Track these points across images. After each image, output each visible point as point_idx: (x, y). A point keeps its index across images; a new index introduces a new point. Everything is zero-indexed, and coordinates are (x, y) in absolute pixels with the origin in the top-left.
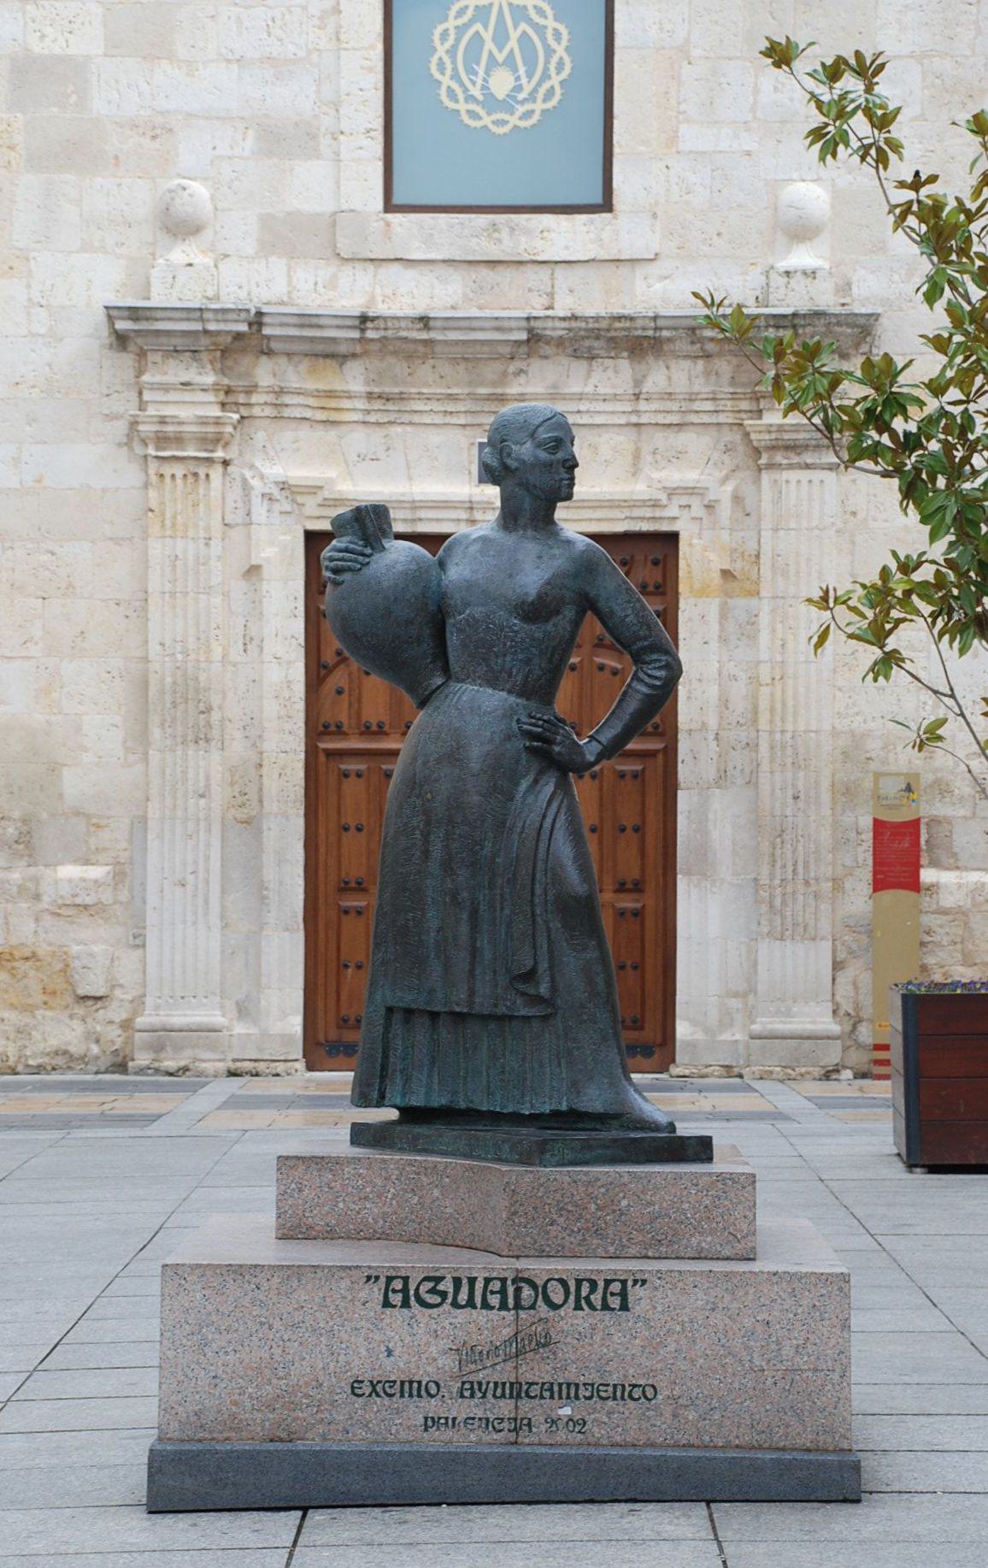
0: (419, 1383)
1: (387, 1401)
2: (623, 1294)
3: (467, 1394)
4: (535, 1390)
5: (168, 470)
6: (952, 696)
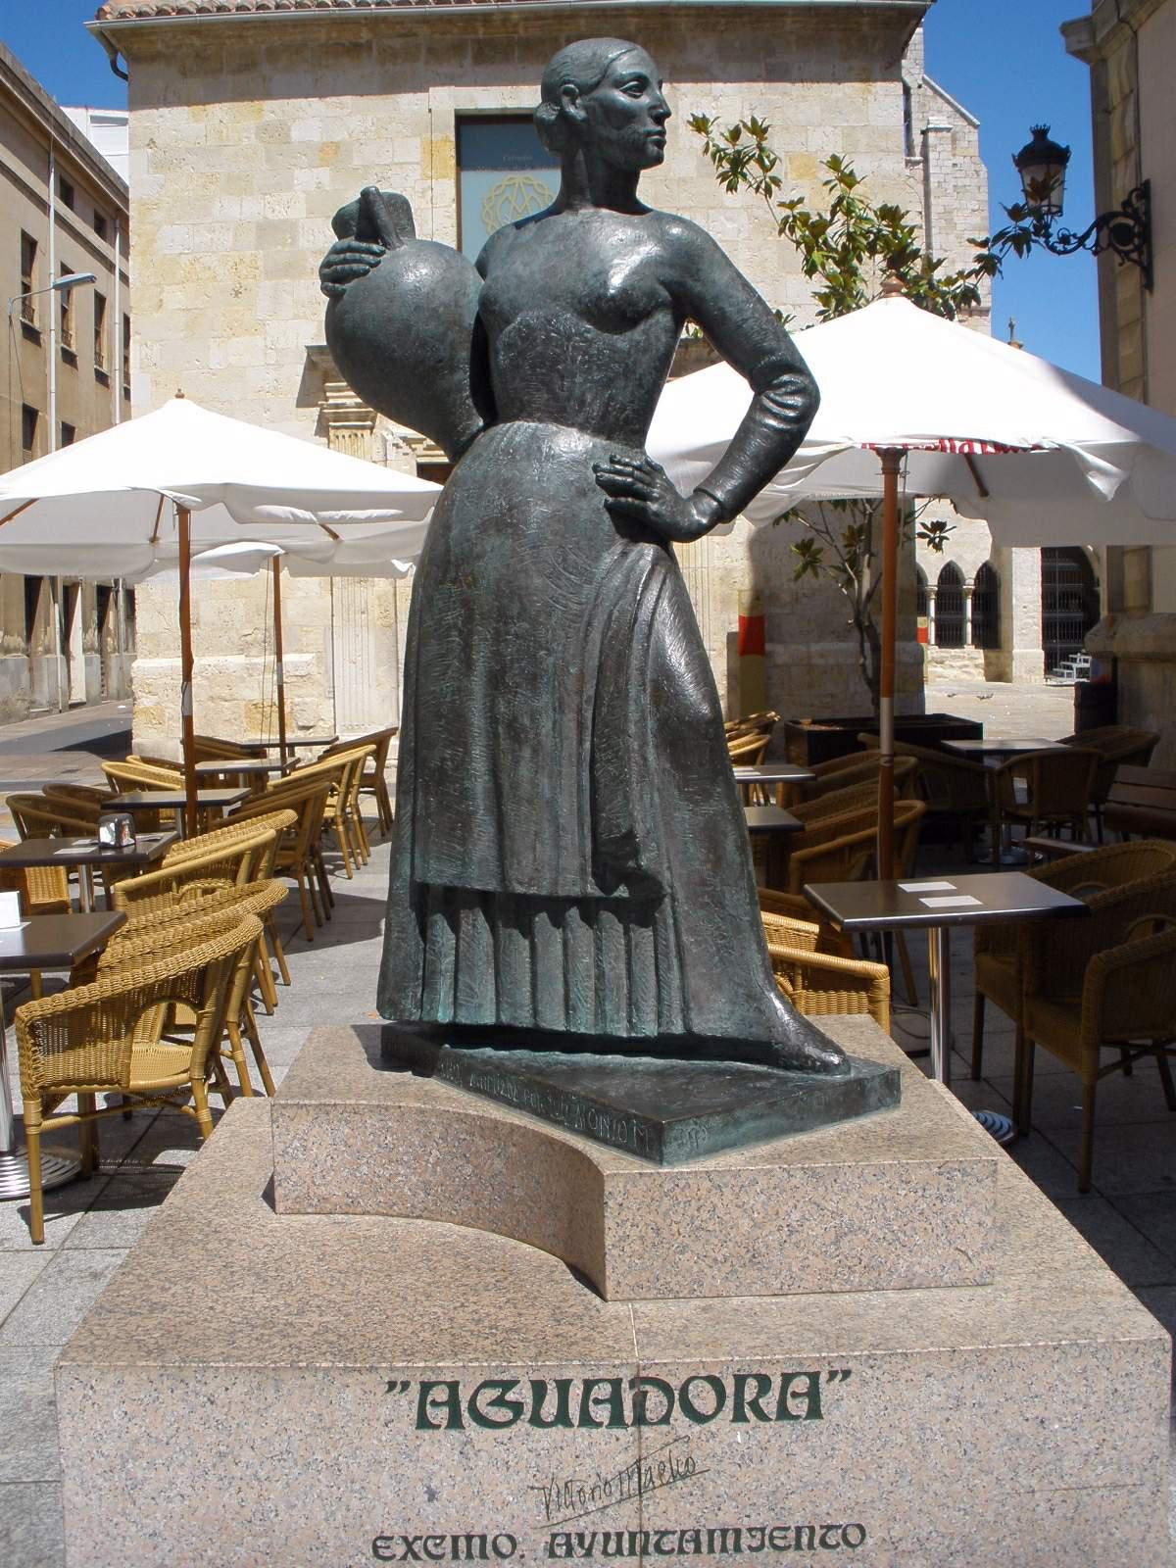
0: (483, 1538)
2: (813, 1394)
5: (340, 433)
6: (828, 533)
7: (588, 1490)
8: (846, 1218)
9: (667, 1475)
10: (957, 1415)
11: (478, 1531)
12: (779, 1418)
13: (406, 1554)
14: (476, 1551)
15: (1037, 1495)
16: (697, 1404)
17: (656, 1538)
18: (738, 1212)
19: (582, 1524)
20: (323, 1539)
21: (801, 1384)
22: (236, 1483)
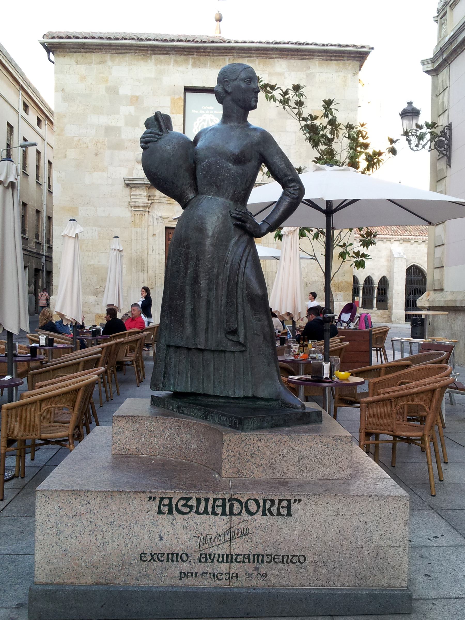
0: (177, 554)
1: (159, 564)
2: (289, 507)
3: (203, 560)
4: (240, 558)
5: (136, 213)
6: (315, 256)
7: (213, 538)
8: (302, 453)
9: (240, 534)
10: (337, 518)
11: (176, 552)
12: (277, 515)
13: (151, 560)
14: (175, 559)
15: (364, 549)
16: (250, 508)
17: (235, 557)
18: (266, 449)
19: (211, 551)
20: (123, 553)
21: (285, 504)
22: (95, 532)
